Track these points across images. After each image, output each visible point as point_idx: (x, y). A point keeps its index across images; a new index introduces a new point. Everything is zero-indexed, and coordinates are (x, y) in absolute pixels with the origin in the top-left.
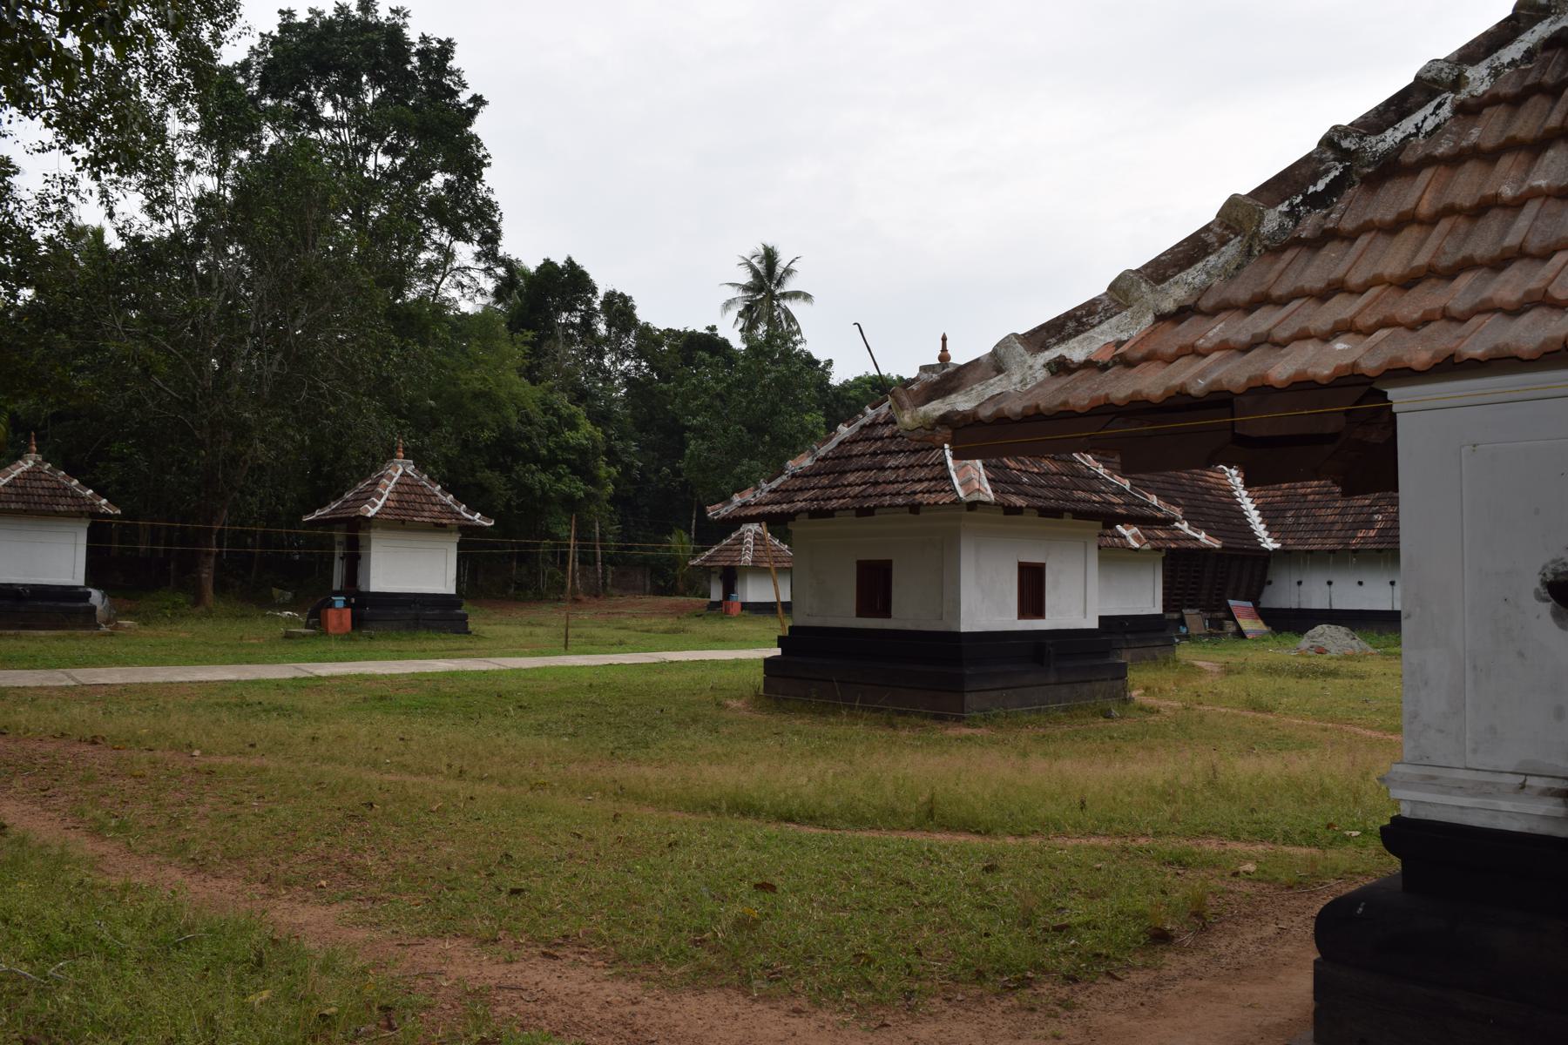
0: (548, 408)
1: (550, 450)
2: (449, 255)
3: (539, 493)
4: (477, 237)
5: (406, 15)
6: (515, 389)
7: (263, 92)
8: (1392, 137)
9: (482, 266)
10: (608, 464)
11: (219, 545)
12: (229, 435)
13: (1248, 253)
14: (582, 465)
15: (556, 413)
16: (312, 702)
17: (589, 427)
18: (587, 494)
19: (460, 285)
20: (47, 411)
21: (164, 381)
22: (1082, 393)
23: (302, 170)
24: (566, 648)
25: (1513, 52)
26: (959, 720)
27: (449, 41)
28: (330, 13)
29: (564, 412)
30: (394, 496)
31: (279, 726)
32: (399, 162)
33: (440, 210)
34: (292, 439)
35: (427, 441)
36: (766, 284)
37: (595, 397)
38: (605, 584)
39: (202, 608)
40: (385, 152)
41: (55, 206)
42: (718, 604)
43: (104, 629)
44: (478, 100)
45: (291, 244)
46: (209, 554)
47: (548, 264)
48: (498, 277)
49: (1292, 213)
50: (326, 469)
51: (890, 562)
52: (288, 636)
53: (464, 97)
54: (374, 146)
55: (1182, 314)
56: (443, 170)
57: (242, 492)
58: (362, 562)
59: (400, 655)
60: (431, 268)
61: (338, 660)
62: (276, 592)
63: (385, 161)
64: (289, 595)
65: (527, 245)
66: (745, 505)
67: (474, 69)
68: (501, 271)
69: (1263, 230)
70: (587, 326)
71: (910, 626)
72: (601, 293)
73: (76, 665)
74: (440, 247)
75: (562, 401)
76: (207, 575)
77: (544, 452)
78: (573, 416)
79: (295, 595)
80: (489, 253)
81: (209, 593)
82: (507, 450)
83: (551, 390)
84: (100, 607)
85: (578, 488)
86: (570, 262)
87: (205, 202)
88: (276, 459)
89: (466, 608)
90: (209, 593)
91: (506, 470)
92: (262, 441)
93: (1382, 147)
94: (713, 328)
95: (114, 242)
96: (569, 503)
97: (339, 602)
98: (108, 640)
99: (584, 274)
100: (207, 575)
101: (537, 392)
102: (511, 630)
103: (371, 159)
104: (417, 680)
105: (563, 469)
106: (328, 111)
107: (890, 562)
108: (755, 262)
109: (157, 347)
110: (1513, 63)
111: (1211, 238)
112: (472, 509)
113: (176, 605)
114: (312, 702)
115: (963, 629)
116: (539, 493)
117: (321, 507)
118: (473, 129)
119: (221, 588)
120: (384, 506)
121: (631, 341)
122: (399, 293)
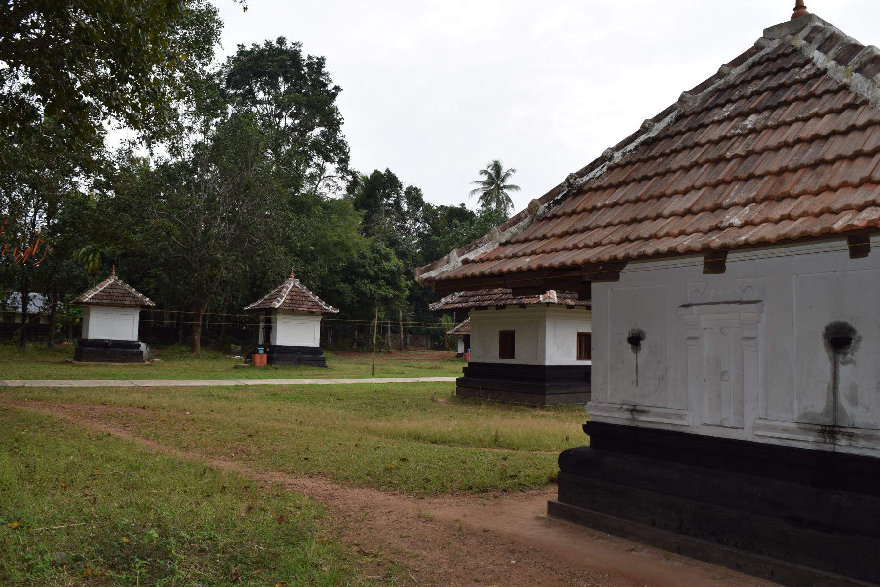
0: (374, 250)
1: (375, 272)
2: (322, 170)
3: (369, 295)
4: (337, 160)
5: (300, 46)
6: (356, 240)
7: (228, 87)
8: (586, 178)
9: (340, 175)
10: (406, 280)
11: (204, 320)
12: (209, 265)
13: (532, 221)
14: (392, 280)
15: (378, 252)
16: (241, 395)
17: (396, 260)
18: (395, 296)
19: (328, 185)
20: (119, 252)
21: (177, 239)
22: (476, 270)
23: (246, 130)
24: (373, 375)
25: (631, 147)
26: (542, 408)
27: (323, 58)
28: (262, 46)
29: (383, 252)
30: (289, 297)
31: (225, 403)
32: (297, 122)
33: (316, 146)
34: (241, 267)
35: (310, 268)
36: (495, 181)
37: (399, 243)
38: (406, 344)
39: (194, 354)
40: (291, 116)
41: (127, 155)
42: (462, 355)
43: (147, 362)
44: (337, 89)
45: (240, 169)
46: (198, 326)
47: (376, 172)
48: (348, 181)
49: (549, 208)
50: (258, 282)
51: (514, 332)
52: (236, 367)
53: (330, 87)
54: (284, 114)
55: (507, 243)
56: (319, 125)
57: (215, 294)
58: (273, 331)
59: (289, 377)
60: (313, 177)
61: (258, 378)
62: (233, 346)
63: (289, 121)
64: (239, 348)
65: (363, 163)
66: (447, 304)
67: (335, 73)
68: (349, 178)
69: (538, 213)
70: (397, 203)
71: (523, 363)
72: (405, 189)
73: (134, 378)
74: (318, 165)
75: (382, 246)
76: (197, 337)
77: (372, 273)
78: (389, 253)
79: (243, 348)
80: (343, 167)
81: (198, 346)
82: (352, 273)
83: (376, 241)
84: (145, 352)
85: (390, 292)
86: (388, 171)
87: (198, 147)
88: (233, 277)
89: (325, 354)
90: (198, 346)
91: (351, 282)
92: (226, 268)
93: (581, 182)
94: (463, 205)
95: (153, 167)
96: (385, 300)
97: (261, 350)
98: (149, 368)
99: (395, 177)
100: (197, 337)
101: (369, 241)
102: (349, 367)
103: (283, 121)
104: (293, 387)
105: (382, 282)
106: (260, 96)
107: (514, 332)
108: (489, 170)
109: (175, 222)
110: (630, 150)
111: (523, 215)
112: (328, 304)
113: (182, 352)
114: (241, 395)
115: (547, 364)
116: (369, 295)
117: (253, 303)
118: (335, 104)
119: (205, 344)
120: (284, 302)
121: (420, 213)
122: (297, 190)
